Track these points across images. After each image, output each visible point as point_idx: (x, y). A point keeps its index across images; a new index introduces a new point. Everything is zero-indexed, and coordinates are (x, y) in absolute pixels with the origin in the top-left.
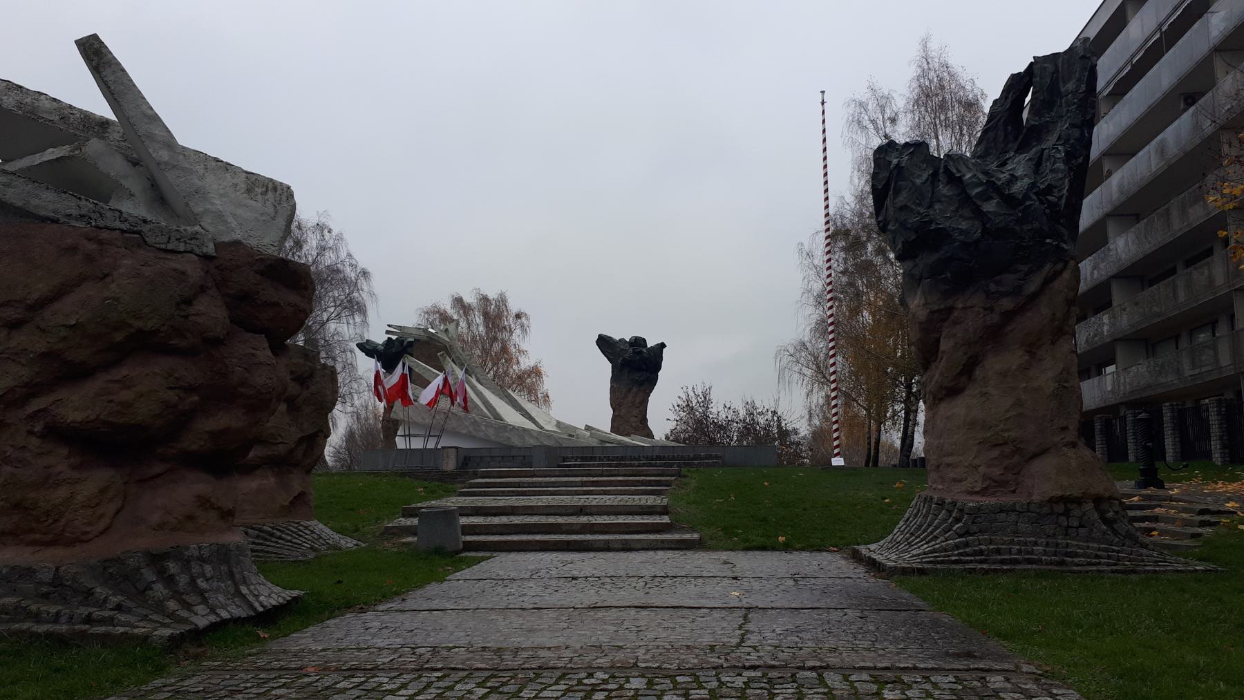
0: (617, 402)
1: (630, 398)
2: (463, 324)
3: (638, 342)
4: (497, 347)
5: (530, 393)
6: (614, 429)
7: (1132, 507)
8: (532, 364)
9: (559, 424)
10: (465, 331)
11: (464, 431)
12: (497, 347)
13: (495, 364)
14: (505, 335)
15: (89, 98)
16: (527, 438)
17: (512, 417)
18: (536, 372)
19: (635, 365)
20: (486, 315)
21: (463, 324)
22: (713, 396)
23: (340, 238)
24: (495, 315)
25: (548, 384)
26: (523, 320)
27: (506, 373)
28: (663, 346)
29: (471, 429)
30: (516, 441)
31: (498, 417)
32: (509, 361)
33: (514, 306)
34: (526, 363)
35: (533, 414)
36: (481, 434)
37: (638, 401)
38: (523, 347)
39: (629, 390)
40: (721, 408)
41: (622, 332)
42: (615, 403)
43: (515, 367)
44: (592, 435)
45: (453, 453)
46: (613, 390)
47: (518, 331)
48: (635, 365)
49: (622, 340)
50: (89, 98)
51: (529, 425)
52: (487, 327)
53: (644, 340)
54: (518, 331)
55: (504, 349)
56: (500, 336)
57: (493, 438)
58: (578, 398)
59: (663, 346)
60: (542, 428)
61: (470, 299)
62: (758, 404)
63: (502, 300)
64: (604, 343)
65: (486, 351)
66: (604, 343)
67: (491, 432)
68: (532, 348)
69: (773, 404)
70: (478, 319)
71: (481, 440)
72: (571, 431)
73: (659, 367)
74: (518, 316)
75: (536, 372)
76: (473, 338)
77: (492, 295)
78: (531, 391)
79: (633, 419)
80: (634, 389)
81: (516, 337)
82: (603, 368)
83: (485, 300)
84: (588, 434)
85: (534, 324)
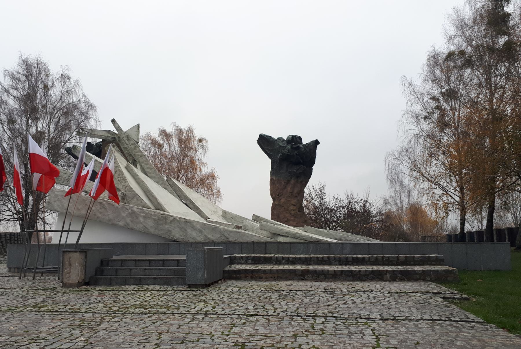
0: (276, 192)
1: (289, 188)
2: (166, 146)
3: (295, 140)
4: (187, 161)
5: (208, 189)
6: (276, 215)
7: (26, 172)
8: (209, 170)
9: (225, 214)
10: (168, 150)
11: (121, 223)
12: (187, 161)
13: (186, 171)
14: (192, 153)
15: (112, 128)
16: (189, 230)
17: (174, 207)
18: (212, 176)
19: (291, 159)
20: (180, 141)
21: (166, 146)
22: (326, 191)
23: (77, 83)
24: (186, 140)
25: (220, 184)
26: (204, 143)
27: (193, 177)
28: (317, 142)
29: (128, 220)
30: (177, 234)
31: (159, 207)
32: (195, 169)
33: (198, 134)
34: (205, 171)
35: (198, 204)
36: (139, 227)
37: (296, 191)
38: (204, 160)
39: (288, 182)
40: (332, 198)
41: (280, 132)
42: (275, 193)
43: (199, 173)
44: (262, 228)
45: (76, 258)
46: (272, 183)
47: (200, 151)
48: (291, 159)
49: (280, 139)
50: (112, 128)
51: (192, 216)
52: (181, 147)
53: (300, 138)
54: (200, 151)
55: (192, 162)
56: (189, 153)
57: (152, 230)
58: (242, 192)
59: (317, 142)
60: (206, 218)
61: (170, 130)
62: (355, 197)
63: (190, 130)
64: (265, 142)
65: (181, 164)
66: (265, 142)
67: (150, 223)
68: (209, 161)
69: (365, 196)
70: (175, 141)
71: (139, 232)
72: (238, 223)
73: (313, 162)
74: (200, 140)
75: (212, 176)
76: (172, 155)
77: (184, 127)
78: (209, 188)
79: (292, 207)
80: (293, 181)
81: (200, 154)
82: (264, 164)
83: (180, 131)
84: (257, 225)
85: (211, 145)
